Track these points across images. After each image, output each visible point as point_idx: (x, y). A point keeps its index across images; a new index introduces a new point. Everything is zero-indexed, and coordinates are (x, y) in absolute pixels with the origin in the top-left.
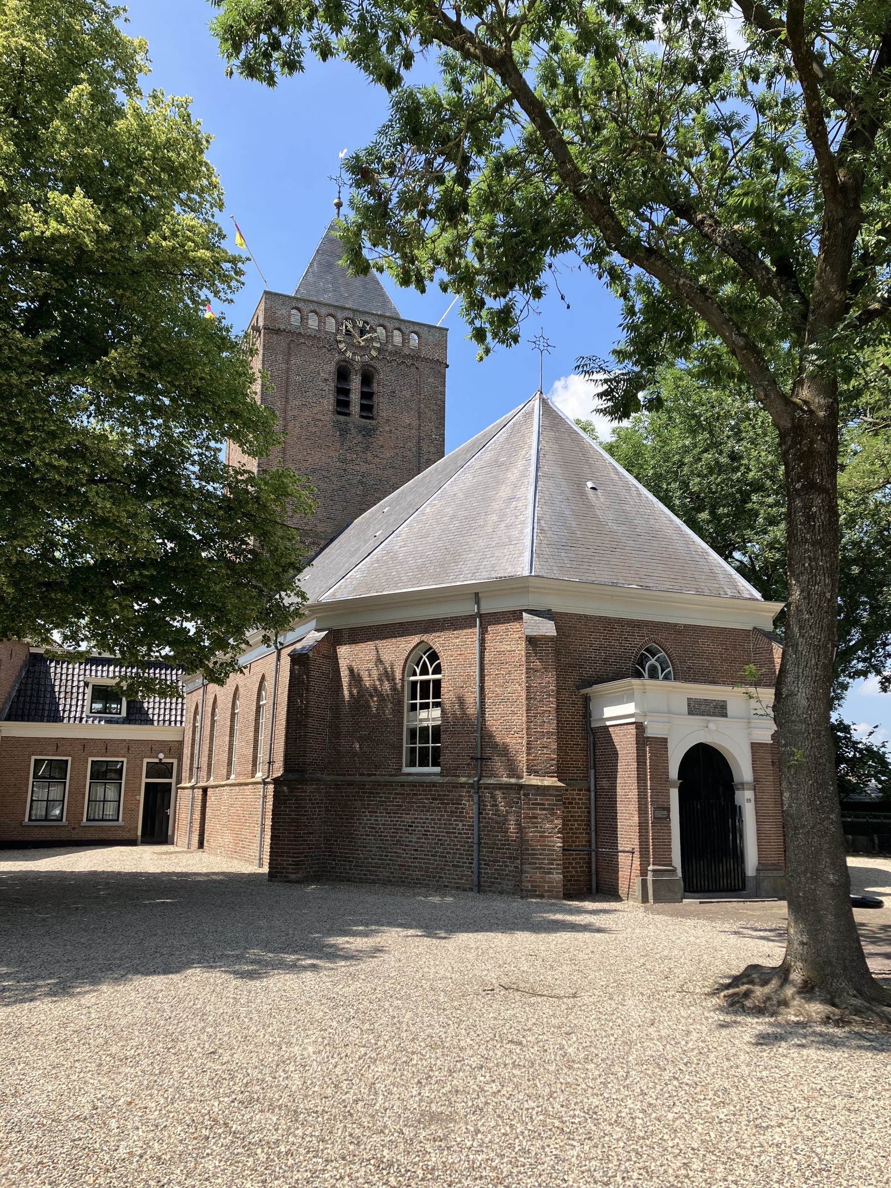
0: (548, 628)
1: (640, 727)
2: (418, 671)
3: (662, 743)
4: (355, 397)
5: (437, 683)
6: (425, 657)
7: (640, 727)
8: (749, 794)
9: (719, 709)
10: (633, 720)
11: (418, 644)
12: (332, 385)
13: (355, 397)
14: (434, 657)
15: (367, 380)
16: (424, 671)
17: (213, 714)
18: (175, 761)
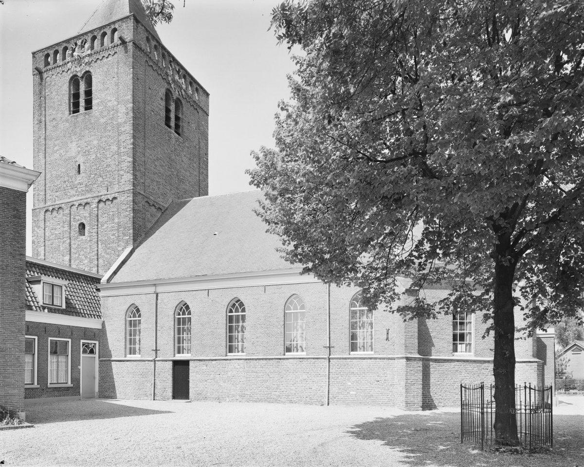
16: (237, 311)
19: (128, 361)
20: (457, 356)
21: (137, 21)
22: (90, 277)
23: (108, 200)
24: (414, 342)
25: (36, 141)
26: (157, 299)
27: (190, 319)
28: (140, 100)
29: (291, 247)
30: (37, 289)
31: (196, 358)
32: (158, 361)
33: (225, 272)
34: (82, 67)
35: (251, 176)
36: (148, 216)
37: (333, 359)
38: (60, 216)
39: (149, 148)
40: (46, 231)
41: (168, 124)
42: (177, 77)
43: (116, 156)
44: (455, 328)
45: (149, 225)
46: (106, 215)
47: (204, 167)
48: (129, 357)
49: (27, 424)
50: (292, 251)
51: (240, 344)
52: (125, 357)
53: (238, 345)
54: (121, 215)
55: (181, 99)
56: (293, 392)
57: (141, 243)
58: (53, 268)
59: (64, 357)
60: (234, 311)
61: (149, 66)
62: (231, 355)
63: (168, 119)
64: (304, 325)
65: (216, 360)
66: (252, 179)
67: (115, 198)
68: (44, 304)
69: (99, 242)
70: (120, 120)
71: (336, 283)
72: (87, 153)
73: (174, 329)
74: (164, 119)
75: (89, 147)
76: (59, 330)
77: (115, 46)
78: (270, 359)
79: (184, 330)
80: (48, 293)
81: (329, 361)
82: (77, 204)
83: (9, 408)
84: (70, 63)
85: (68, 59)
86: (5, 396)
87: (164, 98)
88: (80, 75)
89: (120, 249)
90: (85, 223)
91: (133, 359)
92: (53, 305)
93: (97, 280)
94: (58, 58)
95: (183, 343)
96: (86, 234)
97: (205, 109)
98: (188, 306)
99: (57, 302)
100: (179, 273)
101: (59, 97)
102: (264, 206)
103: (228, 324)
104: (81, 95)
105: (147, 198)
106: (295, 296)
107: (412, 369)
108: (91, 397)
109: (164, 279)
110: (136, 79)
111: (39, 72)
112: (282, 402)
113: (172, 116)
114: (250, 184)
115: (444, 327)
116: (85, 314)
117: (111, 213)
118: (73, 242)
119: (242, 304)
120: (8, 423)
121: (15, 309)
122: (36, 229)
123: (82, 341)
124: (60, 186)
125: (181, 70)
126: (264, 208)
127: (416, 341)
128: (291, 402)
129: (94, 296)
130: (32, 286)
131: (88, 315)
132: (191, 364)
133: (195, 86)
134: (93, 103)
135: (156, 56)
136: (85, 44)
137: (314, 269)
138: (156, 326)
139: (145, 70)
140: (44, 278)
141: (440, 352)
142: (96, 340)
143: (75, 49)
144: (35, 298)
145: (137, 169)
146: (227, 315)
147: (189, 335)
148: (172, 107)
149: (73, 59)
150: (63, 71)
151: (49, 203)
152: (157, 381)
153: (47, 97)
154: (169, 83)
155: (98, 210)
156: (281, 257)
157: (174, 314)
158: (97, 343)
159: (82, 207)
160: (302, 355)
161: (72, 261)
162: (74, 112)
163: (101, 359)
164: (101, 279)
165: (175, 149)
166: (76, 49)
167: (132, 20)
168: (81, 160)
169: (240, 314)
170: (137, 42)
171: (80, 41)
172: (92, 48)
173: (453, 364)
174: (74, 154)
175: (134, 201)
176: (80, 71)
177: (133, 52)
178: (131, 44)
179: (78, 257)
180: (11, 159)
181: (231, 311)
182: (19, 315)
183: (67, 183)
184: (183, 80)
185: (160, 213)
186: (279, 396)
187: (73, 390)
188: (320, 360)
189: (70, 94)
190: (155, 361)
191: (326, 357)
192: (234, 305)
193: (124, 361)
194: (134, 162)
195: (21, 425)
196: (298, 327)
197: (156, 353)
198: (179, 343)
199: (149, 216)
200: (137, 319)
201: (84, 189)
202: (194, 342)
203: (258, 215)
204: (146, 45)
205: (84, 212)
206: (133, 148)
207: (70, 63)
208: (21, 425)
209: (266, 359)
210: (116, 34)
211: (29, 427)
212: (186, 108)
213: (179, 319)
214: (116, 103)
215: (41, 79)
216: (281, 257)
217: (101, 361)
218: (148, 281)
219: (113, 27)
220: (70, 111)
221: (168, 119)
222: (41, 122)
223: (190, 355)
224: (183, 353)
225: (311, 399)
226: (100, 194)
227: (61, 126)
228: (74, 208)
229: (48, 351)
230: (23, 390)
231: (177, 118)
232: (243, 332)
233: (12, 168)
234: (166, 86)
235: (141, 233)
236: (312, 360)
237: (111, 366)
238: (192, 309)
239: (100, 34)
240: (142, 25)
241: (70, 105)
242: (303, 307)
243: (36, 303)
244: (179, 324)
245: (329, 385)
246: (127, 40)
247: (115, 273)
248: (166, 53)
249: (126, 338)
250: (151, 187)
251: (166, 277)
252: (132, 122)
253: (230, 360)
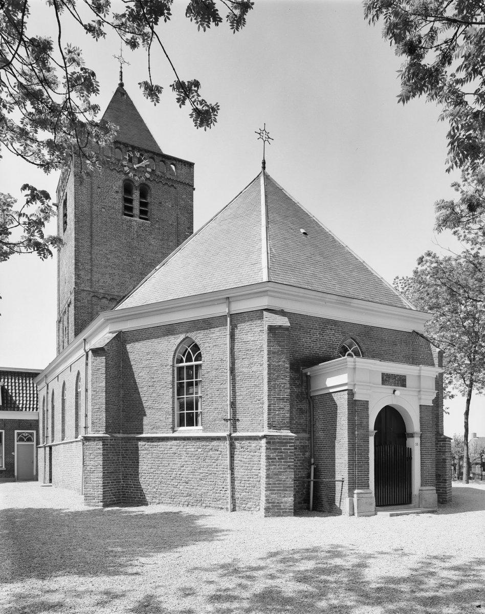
0: (284, 322)
1: (351, 393)
2: (184, 359)
3: (365, 404)
4: (136, 205)
5: (198, 367)
6: (189, 349)
7: (351, 393)
8: (417, 440)
9: (401, 381)
10: (346, 388)
11: (184, 339)
12: (120, 196)
13: (136, 205)
14: (196, 348)
15: (143, 194)
16: (189, 359)
17: (53, 402)
18: (35, 432)
20: (181, 431)
24: (101, 417)
44: (180, 392)
47: (82, 273)
107: (91, 452)
115: (161, 392)
127: (104, 415)
141: (158, 428)
173: (169, 443)
244: (180, 377)
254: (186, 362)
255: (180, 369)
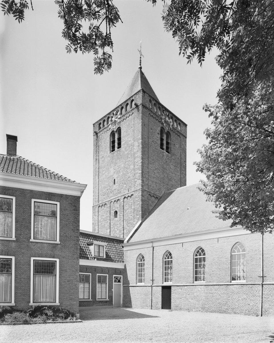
16: (200, 255)
19: (137, 286)
21: (144, 92)
22: (119, 240)
23: (129, 196)
25: (95, 170)
26: (153, 250)
27: (171, 261)
28: (146, 137)
29: (222, 209)
30: (92, 248)
31: (175, 285)
32: (154, 286)
33: (193, 231)
34: (116, 125)
35: (197, 166)
36: (151, 201)
37: (265, 284)
38: (106, 209)
39: (151, 164)
40: (99, 217)
41: (162, 148)
42: (167, 119)
43: (133, 171)
45: (151, 208)
46: (128, 205)
47: (145, 179)
48: (139, 284)
49: (80, 320)
50: (223, 212)
51: (202, 275)
52: (163, 284)
53: (201, 276)
54: (135, 204)
55: (170, 131)
56: (237, 306)
57: (146, 219)
58: (100, 237)
59: (105, 284)
60: (198, 255)
61: (151, 116)
62: (196, 283)
63: (162, 145)
64: (245, 262)
65: (187, 286)
66: (198, 168)
67: (132, 195)
68: (95, 256)
69: (124, 221)
70: (135, 151)
71: (260, 231)
72: (118, 172)
73: (163, 267)
74: (160, 145)
75: (119, 169)
76: (102, 270)
77: (132, 110)
78: (221, 285)
79: (168, 268)
80: (97, 250)
81: (262, 286)
82: (113, 201)
83: (71, 311)
84: (111, 125)
85: (110, 123)
86: (70, 305)
87: (160, 133)
88: (115, 130)
89: (135, 223)
90: (117, 211)
91: (139, 285)
92: (99, 256)
93: (122, 242)
94: (105, 124)
95: (168, 276)
96: (118, 217)
97: (184, 135)
98: (171, 253)
99: (101, 255)
100: (166, 234)
101: (105, 145)
102: (205, 184)
103: (195, 264)
104: (116, 141)
105: (149, 192)
106: (237, 244)
108: (119, 306)
109: (157, 238)
110: (143, 125)
111: (96, 133)
112: (229, 313)
113: (165, 142)
114: (197, 171)
116: (116, 261)
117: (130, 204)
118: (111, 222)
119: (203, 251)
120: (70, 320)
121: (75, 259)
122: (94, 217)
123: (114, 276)
124: (105, 192)
125: (170, 114)
126: (204, 185)
128: (235, 313)
129: (121, 251)
130: (89, 247)
131: (117, 261)
132: (172, 288)
133: (178, 122)
134: (122, 144)
135: (155, 109)
136: (117, 113)
137: (240, 223)
138: (153, 266)
139: (149, 119)
140: (95, 242)
142: (96, 275)
143: (113, 117)
144: (90, 253)
145: (144, 176)
146: (194, 258)
147: (172, 271)
148: (165, 137)
149: (112, 122)
150: (107, 130)
151: (100, 202)
152: (153, 298)
153: (100, 146)
154: (163, 124)
155: (124, 203)
156: (216, 217)
157: (163, 258)
158: (122, 276)
159: (116, 202)
160: (243, 282)
161: (111, 232)
162: (112, 151)
163: (124, 285)
164: (124, 241)
165: (166, 161)
166: (114, 117)
167: (141, 92)
168: (115, 176)
169: (202, 256)
170: (144, 104)
171: (115, 112)
172: (121, 113)
174: (112, 174)
175: (142, 195)
176: (115, 128)
177: (142, 110)
178: (141, 105)
179: (114, 230)
180: (73, 180)
181: (196, 255)
182: (76, 262)
183: (109, 190)
184: (171, 120)
185: (157, 200)
186: (227, 309)
187: (109, 303)
188: (256, 286)
189: (110, 142)
190: (152, 286)
191: (260, 283)
192: (199, 251)
193: (135, 286)
194: (142, 173)
195: (77, 321)
196: (241, 264)
197: (153, 282)
198: (166, 276)
199: (151, 203)
200: (143, 262)
201: (117, 192)
202: (174, 275)
203: (200, 191)
204: (149, 104)
205: (117, 205)
206: (142, 165)
207: (111, 125)
208: (77, 321)
209: (218, 285)
210: (133, 103)
211: (80, 322)
212: (173, 136)
213: (166, 261)
214: (133, 141)
215: (97, 137)
216: (216, 217)
217: (124, 287)
218: (149, 240)
219: (131, 99)
220: (110, 151)
221: (162, 145)
222: (97, 160)
223: (171, 283)
224: (168, 282)
225: (249, 311)
226: (125, 194)
227: (106, 160)
228: (112, 203)
229: (96, 281)
230: (78, 302)
231: (168, 143)
232: (204, 268)
233: (74, 184)
234: (161, 125)
235: (146, 212)
236: (250, 285)
237: (129, 289)
238: (173, 255)
239: (125, 105)
240: (147, 94)
241: (110, 148)
242: (244, 250)
243: (91, 256)
245: (262, 302)
246: (139, 104)
247: (131, 237)
248: (161, 107)
249: (136, 273)
250: (152, 186)
251: (158, 237)
252: (141, 150)
253: (196, 285)
254: (199, 256)
255: (196, 259)
